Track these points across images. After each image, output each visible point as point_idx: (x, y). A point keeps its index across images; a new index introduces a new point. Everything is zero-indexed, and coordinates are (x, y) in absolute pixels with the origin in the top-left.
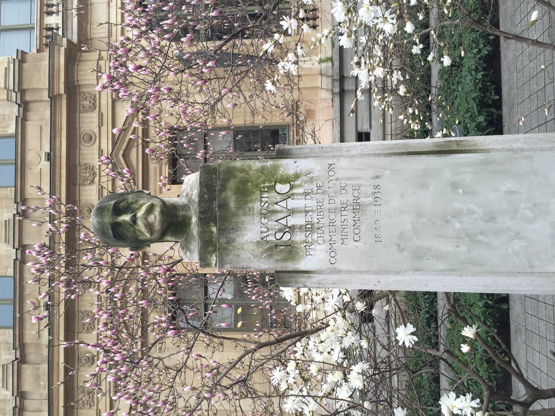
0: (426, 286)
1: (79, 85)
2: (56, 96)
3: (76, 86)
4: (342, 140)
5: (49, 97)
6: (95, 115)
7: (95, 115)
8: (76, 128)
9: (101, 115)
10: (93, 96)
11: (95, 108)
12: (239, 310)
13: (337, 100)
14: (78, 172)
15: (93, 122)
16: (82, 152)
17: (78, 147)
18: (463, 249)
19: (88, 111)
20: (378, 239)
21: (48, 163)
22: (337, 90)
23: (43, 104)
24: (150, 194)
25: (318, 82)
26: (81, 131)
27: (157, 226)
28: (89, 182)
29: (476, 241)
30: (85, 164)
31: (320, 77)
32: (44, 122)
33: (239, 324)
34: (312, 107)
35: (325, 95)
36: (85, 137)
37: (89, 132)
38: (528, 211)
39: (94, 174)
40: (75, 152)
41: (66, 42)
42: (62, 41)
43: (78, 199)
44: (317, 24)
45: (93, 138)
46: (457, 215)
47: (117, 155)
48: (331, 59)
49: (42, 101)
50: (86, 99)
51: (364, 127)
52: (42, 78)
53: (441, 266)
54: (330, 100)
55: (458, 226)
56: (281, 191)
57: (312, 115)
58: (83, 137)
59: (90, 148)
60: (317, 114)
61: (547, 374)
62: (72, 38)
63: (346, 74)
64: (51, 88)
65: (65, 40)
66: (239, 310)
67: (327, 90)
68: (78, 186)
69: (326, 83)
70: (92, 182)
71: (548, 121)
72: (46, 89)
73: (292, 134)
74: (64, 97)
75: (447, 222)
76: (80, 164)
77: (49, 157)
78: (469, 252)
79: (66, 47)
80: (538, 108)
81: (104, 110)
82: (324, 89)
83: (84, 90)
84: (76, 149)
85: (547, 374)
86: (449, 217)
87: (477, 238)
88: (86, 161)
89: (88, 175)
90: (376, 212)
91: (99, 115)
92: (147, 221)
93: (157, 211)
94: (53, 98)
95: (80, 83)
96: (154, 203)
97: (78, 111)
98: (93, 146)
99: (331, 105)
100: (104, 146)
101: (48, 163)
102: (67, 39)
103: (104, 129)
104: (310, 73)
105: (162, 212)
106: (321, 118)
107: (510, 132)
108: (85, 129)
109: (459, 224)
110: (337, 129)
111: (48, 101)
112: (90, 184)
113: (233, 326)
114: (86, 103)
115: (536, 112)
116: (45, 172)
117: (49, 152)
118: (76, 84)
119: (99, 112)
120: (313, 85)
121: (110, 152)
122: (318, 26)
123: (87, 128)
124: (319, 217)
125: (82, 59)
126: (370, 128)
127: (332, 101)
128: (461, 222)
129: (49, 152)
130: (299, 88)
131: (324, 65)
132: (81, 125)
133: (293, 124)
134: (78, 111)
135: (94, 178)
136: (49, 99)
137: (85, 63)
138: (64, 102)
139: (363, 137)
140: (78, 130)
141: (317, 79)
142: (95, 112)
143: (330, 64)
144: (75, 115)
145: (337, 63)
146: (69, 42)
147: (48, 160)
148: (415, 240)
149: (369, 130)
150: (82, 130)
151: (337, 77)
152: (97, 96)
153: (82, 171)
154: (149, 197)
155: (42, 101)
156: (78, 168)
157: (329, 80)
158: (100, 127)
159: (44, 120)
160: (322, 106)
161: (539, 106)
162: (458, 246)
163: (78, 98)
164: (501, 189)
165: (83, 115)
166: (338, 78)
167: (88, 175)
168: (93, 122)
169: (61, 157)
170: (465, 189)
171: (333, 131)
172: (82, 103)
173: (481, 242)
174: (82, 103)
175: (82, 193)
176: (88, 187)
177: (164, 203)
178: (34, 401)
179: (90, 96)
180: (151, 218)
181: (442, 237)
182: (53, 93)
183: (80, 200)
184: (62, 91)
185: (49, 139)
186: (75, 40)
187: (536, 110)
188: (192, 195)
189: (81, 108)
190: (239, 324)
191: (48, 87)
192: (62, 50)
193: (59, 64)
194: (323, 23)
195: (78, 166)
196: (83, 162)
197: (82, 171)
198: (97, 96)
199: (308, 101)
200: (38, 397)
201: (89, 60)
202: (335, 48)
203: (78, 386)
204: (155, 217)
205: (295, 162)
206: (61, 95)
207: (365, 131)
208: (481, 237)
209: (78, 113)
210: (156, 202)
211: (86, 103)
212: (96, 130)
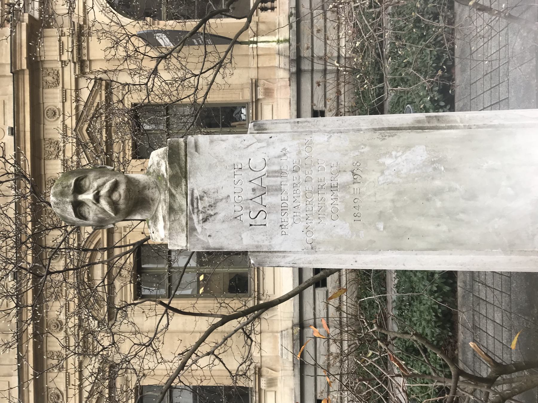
0: (404, 265)
1: (42, 61)
2: (18, 71)
3: (38, 62)
4: (299, 116)
5: (11, 72)
6: (57, 92)
7: (57, 92)
8: (39, 104)
9: (64, 92)
10: (56, 72)
11: (58, 84)
12: (202, 278)
13: (294, 79)
14: (43, 147)
15: (57, 98)
16: (46, 127)
17: (42, 122)
18: (444, 228)
19: (51, 87)
20: (357, 218)
21: (12, 138)
22: (294, 70)
23: (6, 79)
24: (113, 170)
25: (276, 61)
26: (45, 107)
27: (122, 205)
28: (54, 156)
29: (457, 220)
30: (50, 139)
31: (277, 57)
32: (7, 97)
33: (201, 291)
34: (271, 86)
35: (283, 74)
36: (49, 112)
37: (53, 107)
38: (509, 189)
39: (58, 148)
40: (39, 127)
41: (27, 18)
42: (23, 16)
43: (43, 173)
44: (275, 6)
45: (57, 113)
46: (438, 192)
47: (81, 129)
48: (288, 41)
49: (4, 76)
50: (49, 74)
51: (320, 106)
52: (4, 53)
53: (421, 244)
54: (287, 79)
55: (439, 204)
56: (46, 134)
57: (270, 94)
58: (47, 112)
59: (54, 123)
60: (275, 92)
61: (494, 337)
62: (34, 14)
63: (302, 55)
64: (13, 63)
65: (26, 17)
66: (202, 278)
67: (284, 69)
68: (43, 160)
69: (284, 62)
70: (57, 156)
71: (501, 101)
72: (8, 64)
73: (251, 111)
74: (27, 72)
75: (428, 200)
76: (44, 139)
77: (13, 131)
78: (449, 231)
79: (27, 23)
80: (491, 88)
81: (67, 86)
82: (282, 68)
83: (46, 66)
84: (40, 124)
85: (494, 337)
86: (430, 195)
87: (458, 217)
88: (50, 136)
89: (52, 149)
90: (355, 190)
91: (63, 90)
92: (112, 199)
93: (122, 188)
94: (16, 74)
95: (43, 58)
96: (118, 179)
97: (42, 86)
98: (57, 121)
99: (288, 84)
100: (68, 122)
101: (12, 138)
102: (29, 14)
103: (68, 104)
104: (268, 52)
105: (128, 190)
106: (279, 97)
107: (461, 110)
108: (49, 104)
109: (440, 203)
110: (294, 107)
111: (10, 76)
112: (55, 158)
113: (195, 292)
114: (49, 79)
115: (489, 92)
116: (9, 147)
117: (13, 126)
118: (39, 60)
119: (63, 88)
120: (271, 65)
121: (74, 127)
122: (276, 8)
123: (51, 104)
124: (295, 195)
125: (45, 34)
126: (325, 106)
127: (290, 80)
128: (442, 200)
129: (13, 126)
130: (258, 67)
131: (282, 46)
132: (45, 101)
133: (253, 102)
134: (42, 86)
135: (58, 152)
136: (12, 74)
137: (49, 39)
138: (27, 77)
139: (316, 114)
140: (42, 105)
141: (275, 59)
142: (58, 87)
143: (287, 44)
144: (39, 91)
145: (294, 44)
146: (31, 17)
147: (12, 134)
148: (395, 219)
149: (324, 109)
150: (45, 105)
151: (293, 57)
152: (60, 72)
153: (46, 146)
154: (113, 172)
155: (4, 76)
156: (43, 143)
157: (287, 60)
158: (63, 103)
159: (6, 95)
160: (279, 85)
161: (492, 86)
162: (438, 225)
163: (41, 73)
164: (482, 166)
165: (46, 91)
166: (295, 58)
167: (52, 149)
168: (57, 98)
169: (25, 131)
170: (446, 167)
171: (290, 109)
172: (45, 78)
173: (462, 220)
174: (45, 78)
175: (47, 167)
176: (53, 162)
177: (130, 182)
178: (4, 366)
179: (52, 72)
180: (115, 196)
181: (423, 215)
182: (15, 68)
183: (45, 174)
184: (25, 67)
185: (12, 114)
186: (36, 15)
187: (490, 89)
188: (159, 170)
189: (45, 83)
190: (201, 291)
191: (9, 62)
192: (24, 25)
193: (21, 40)
194: (281, 5)
195: (43, 141)
196: (47, 136)
197: (46, 146)
198: (60, 72)
199: (266, 80)
200: (8, 363)
201: (52, 36)
202: (293, 29)
203: (47, 351)
204: (120, 195)
205: (271, 138)
206: (24, 70)
207: (321, 109)
208: (462, 216)
209: (41, 89)
210: (121, 178)
211: (49, 79)
212: (60, 106)
